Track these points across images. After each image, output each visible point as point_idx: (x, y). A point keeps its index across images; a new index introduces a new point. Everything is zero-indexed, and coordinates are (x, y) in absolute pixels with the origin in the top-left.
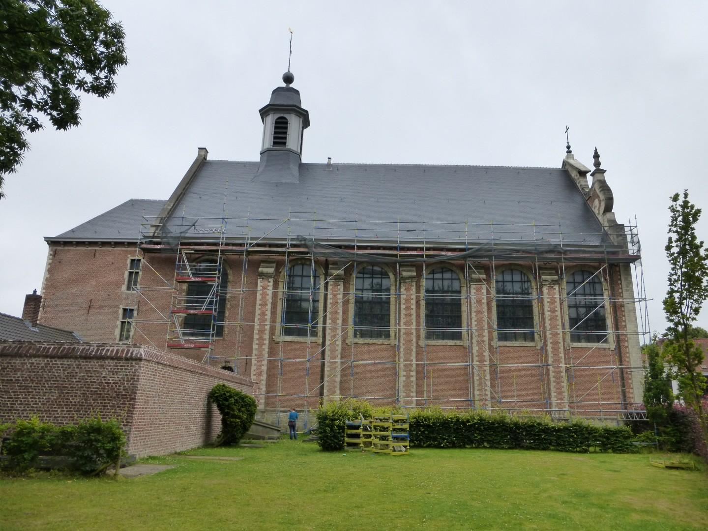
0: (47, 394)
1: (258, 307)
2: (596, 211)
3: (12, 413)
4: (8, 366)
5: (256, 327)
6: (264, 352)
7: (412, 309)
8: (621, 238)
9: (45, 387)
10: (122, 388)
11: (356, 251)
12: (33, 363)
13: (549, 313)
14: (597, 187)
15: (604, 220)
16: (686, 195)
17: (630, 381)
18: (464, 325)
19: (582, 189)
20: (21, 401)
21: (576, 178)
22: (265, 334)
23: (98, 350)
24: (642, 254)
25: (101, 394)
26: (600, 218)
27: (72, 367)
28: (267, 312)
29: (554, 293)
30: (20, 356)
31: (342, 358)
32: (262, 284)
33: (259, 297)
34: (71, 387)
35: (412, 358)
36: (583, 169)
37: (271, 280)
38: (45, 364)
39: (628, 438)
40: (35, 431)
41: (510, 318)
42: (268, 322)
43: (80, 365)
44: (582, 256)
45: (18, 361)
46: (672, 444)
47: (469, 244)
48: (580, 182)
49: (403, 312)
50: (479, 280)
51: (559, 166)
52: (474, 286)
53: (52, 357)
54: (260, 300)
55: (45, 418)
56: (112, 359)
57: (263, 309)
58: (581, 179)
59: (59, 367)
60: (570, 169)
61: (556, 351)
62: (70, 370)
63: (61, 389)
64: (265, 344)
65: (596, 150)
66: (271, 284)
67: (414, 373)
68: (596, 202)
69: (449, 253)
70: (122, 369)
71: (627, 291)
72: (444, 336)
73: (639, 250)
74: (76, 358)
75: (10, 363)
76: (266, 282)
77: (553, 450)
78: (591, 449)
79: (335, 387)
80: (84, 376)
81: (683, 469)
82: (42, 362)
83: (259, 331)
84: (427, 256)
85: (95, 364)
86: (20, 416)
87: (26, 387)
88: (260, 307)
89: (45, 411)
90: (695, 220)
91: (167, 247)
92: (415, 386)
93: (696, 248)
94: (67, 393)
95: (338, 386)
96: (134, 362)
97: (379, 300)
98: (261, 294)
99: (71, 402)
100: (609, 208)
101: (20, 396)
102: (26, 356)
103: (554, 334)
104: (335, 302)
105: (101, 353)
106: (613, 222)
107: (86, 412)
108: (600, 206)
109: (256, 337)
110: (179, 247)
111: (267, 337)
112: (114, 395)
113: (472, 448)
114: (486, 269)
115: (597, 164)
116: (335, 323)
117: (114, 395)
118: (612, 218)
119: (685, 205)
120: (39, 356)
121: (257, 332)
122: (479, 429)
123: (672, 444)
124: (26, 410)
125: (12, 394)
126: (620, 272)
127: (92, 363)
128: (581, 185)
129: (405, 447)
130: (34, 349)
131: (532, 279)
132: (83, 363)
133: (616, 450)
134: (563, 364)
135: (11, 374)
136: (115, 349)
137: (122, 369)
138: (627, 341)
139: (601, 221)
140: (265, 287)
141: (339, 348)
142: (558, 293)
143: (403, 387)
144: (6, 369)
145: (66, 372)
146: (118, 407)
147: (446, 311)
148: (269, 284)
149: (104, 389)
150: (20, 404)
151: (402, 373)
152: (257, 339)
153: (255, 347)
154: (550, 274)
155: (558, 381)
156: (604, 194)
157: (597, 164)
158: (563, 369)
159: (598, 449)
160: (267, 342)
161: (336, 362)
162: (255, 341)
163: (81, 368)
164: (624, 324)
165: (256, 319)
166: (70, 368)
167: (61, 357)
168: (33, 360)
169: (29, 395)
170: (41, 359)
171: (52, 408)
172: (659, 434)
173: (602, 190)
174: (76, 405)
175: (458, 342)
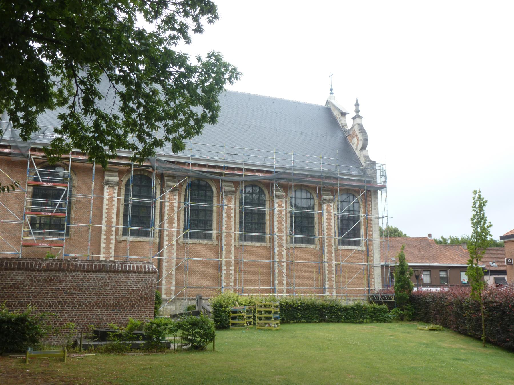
0: (88, 299)
1: (105, 211)
2: (354, 147)
3: (63, 313)
4: (54, 278)
5: (104, 228)
6: (111, 251)
7: (232, 217)
8: (373, 171)
9: (86, 293)
10: (144, 293)
11: (191, 168)
12: (74, 276)
13: (327, 224)
14: (356, 128)
15: (360, 155)
16: (480, 192)
17: (372, 273)
18: (268, 230)
19: (343, 127)
20: (69, 304)
21: (337, 116)
22: (112, 235)
23: (122, 266)
24: (388, 185)
25: (129, 298)
26: (357, 153)
27: (104, 279)
28: (106, 215)
29: (331, 209)
30: (63, 271)
31: (177, 255)
32: (108, 191)
33: (105, 202)
34: (106, 293)
35: (231, 256)
36: (344, 111)
37: (117, 188)
38: (83, 277)
39: (385, 313)
40: (207, 325)
41: (299, 226)
42: (114, 225)
43: (110, 277)
44: (351, 183)
45: (61, 275)
46: (410, 316)
47: (276, 168)
48: (341, 121)
49: (225, 219)
50: (282, 197)
51: (323, 104)
52: (277, 201)
53: (88, 271)
54: (107, 205)
55: (89, 316)
56: (135, 272)
57: (109, 213)
58: (342, 118)
59: (94, 279)
60: (332, 108)
61: (329, 252)
62: (103, 281)
63: (98, 295)
64: (112, 243)
65: (357, 100)
66: (116, 191)
67: (232, 268)
68: (355, 140)
69: (261, 175)
70: (142, 280)
71: (375, 209)
72: (252, 239)
73: (385, 182)
74: (107, 272)
75: (56, 276)
76: (112, 189)
77: (343, 322)
78: (365, 321)
79: (171, 279)
80: (114, 285)
81: (437, 330)
82: (81, 275)
83: (106, 232)
84: (245, 175)
85: (121, 275)
86: (70, 315)
87: (71, 294)
88: (107, 211)
89: (88, 310)
90: (484, 205)
91: (17, 152)
92: (233, 278)
93: (483, 218)
94: (103, 298)
95: (174, 278)
96: (150, 275)
97: (204, 209)
98: (107, 200)
99: (107, 304)
100: (364, 147)
101: (67, 301)
102: (68, 271)
103: (329, 240)
104: (171, 210)
105: (126, 269)
106: (367, 157)
107: (120, 310)
108: (358, 144)
109: (103, 237)
110: (30, 153)
111: (113, 237)
112: (139, 298)
113: (294, 323)
114: (285, 188)
115: (357, 111)
116: (171, 226)
117: (139, 298)
118: (367, 155)
119: (480, 197)
120: (78, 271)
121: (105, 233)
122: (300, 309)
123: (410, 316)
124: (74, 311)
125: (61, 299)
126: (371, 195)
127: (120, 276)
128: (341, 124)
129: (277, 324)
130: (72, 265)
131: (315, 197)
132: (113, 276)
133: (378, 321)
134: (333, 262)
135: (58, 284)
136: (135, 265)
137: (142, 280)
138: (372, 245)
139: (358, 155)
140: (111, 194)
141: (175, 247)
142: (333, 209)
143: (225, 278)
144: (53, 280)
145: (100, 282)
146: (143, 306)
147: (254, 219)
148: (115, 191)
149: (131, 294)
150: (67, 306)
151: (224, 268)
152: (105, 239)
153: (103, 245)
154: (328, 195)
155: (330, 273)
156: (363, 135)
157: (357, 111)
158: (334, 265)
159: (368, 320)
160: (113, 242)
161: (173, 259)
162: (103, 241)
163: (112, 279)
164: (371, 233)
165: (103, 222)
166: (103, 279)
167: (95, 272)
168: (74, 274)
169: (74, 300)
170: (79, 273)
171: (93, 308)
172: (402, 310)
173: (361, 132)
174: (111, 306)
175: (263, 244)
